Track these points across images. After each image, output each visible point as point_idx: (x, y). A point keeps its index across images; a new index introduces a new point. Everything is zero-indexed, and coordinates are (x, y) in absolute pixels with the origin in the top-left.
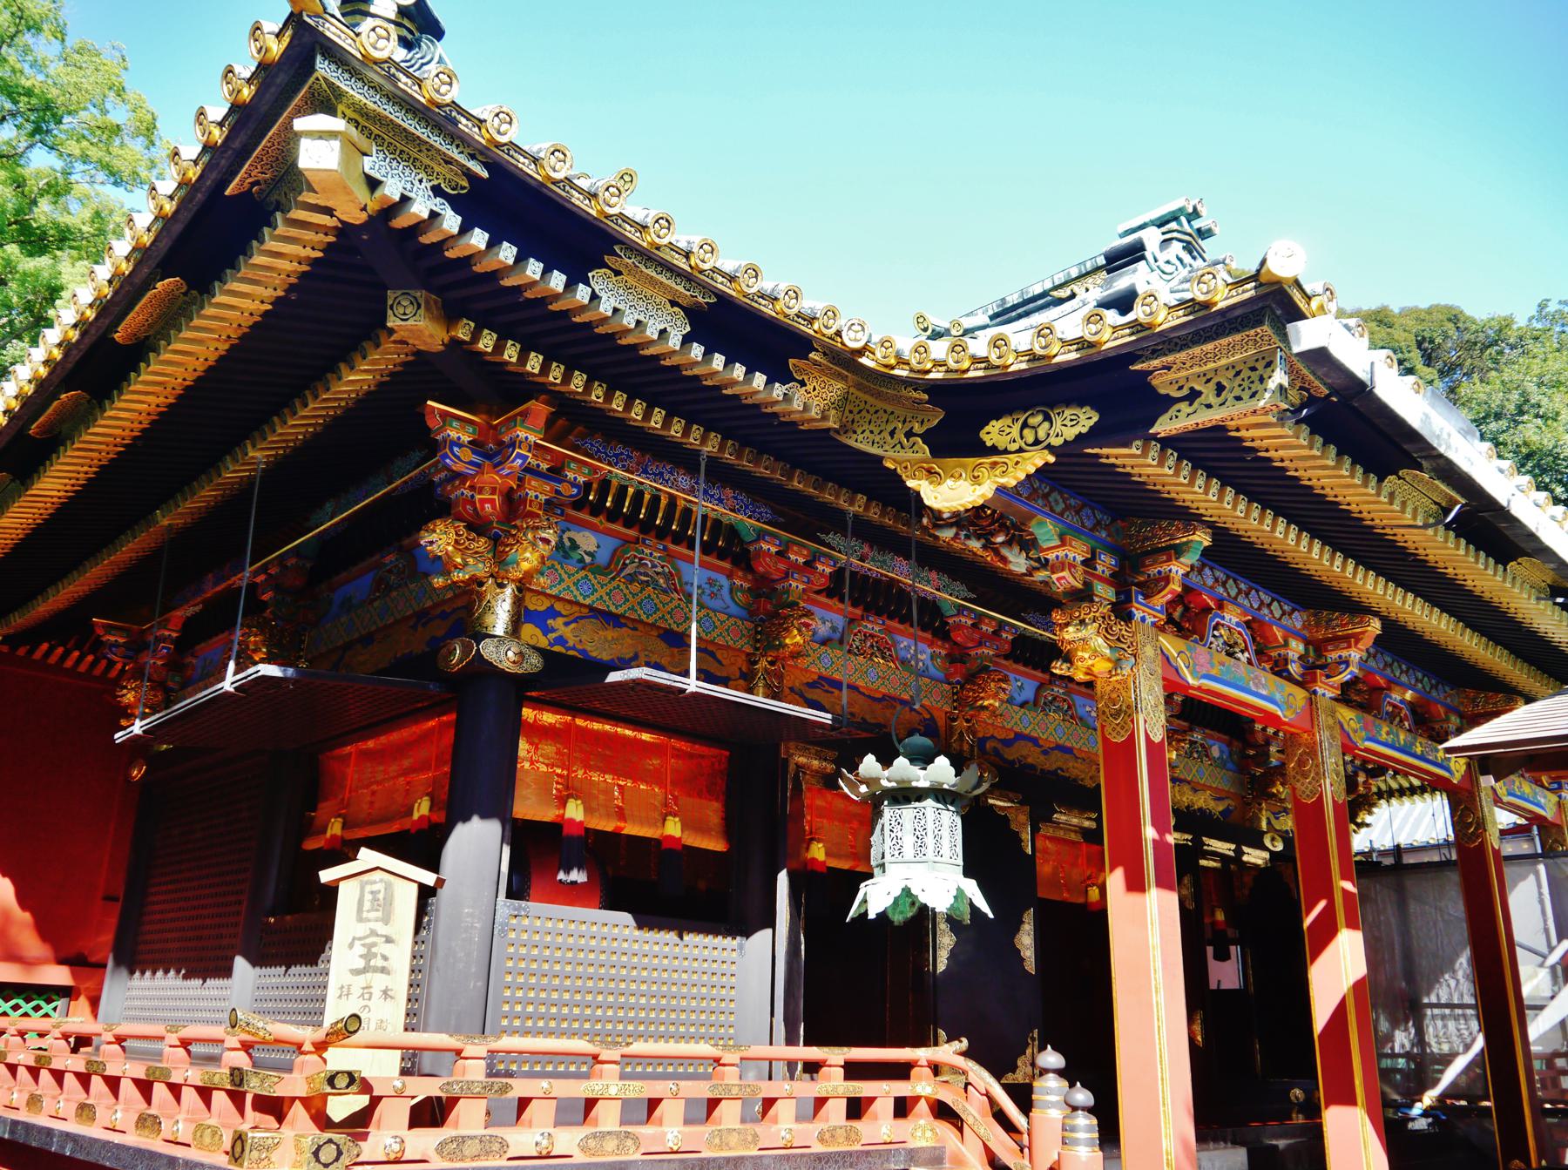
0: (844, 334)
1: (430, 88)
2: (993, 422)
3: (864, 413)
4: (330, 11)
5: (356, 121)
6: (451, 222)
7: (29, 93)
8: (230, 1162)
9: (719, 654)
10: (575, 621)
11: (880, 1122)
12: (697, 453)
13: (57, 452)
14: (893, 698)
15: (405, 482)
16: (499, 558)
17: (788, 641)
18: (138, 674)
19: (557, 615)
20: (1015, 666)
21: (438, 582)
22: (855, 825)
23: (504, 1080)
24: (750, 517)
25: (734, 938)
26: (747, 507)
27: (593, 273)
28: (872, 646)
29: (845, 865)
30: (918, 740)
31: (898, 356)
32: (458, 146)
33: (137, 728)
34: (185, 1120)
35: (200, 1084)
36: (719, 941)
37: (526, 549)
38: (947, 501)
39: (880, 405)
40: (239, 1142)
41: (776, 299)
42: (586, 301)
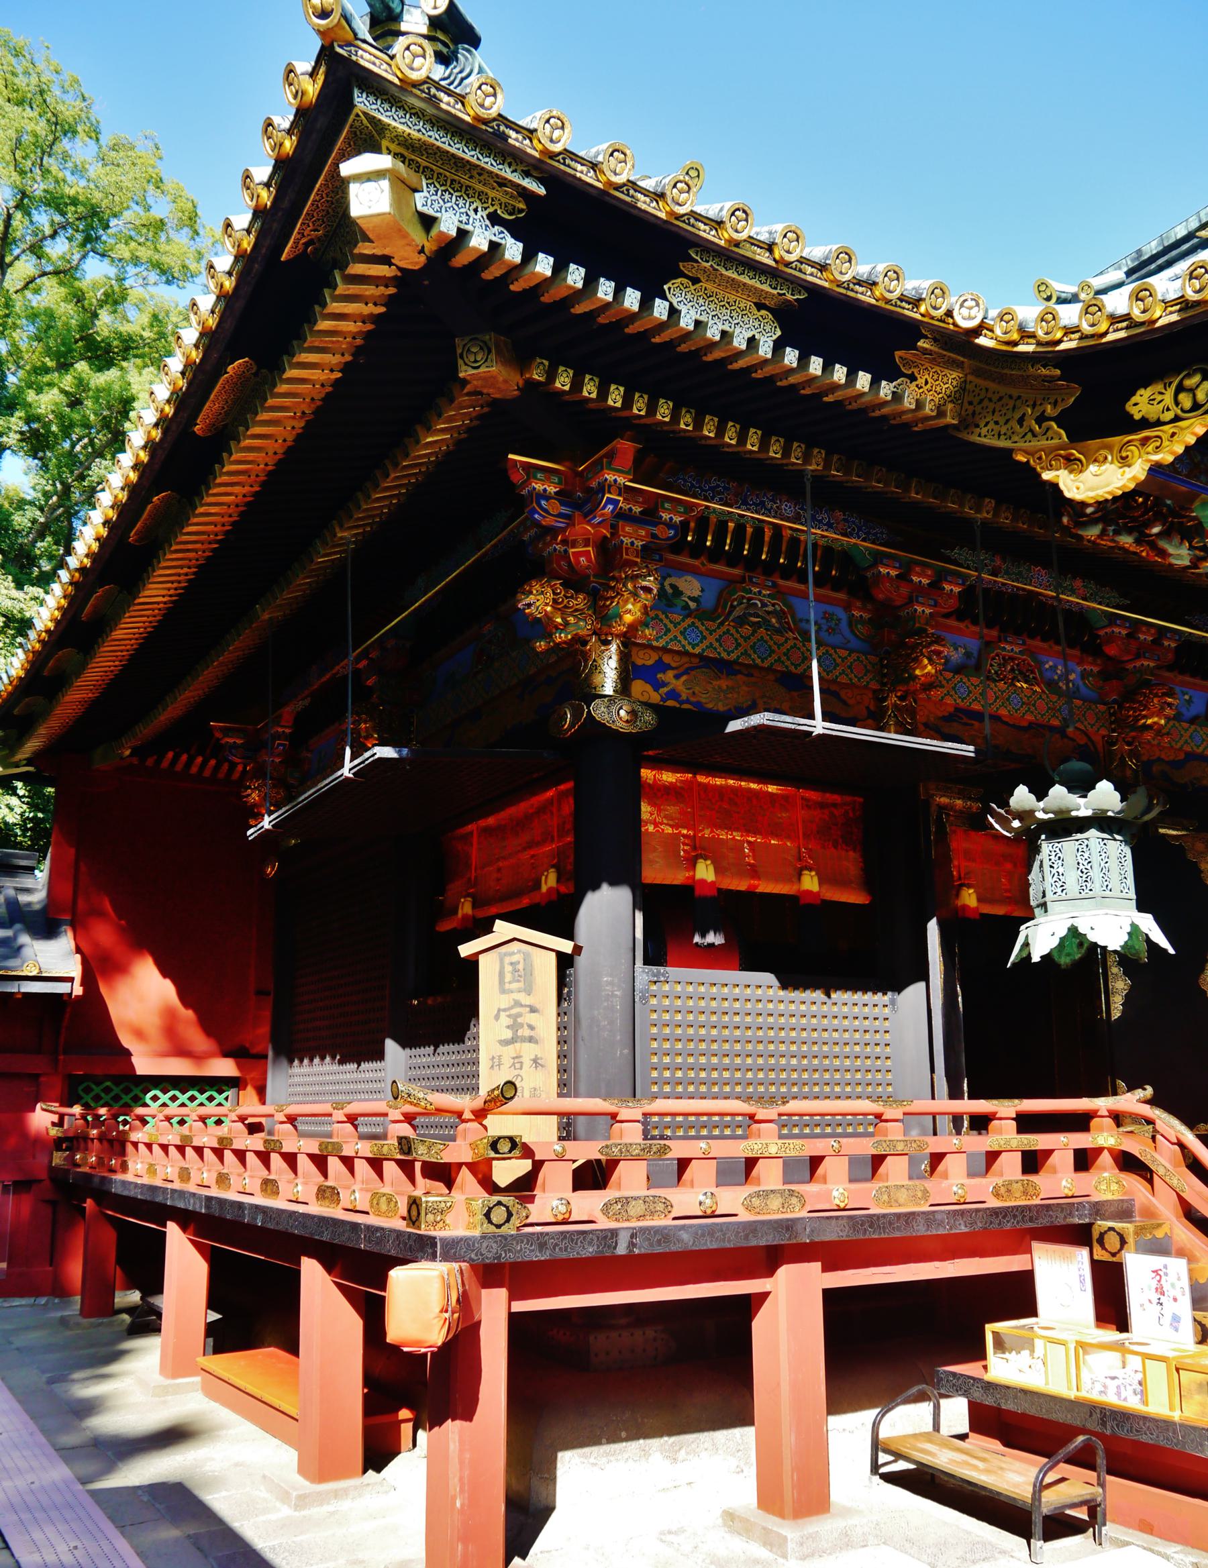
0: (955, 314)
1: (474, 104)
2: (1141, 391)
3: (986, 402)
4: (361, 36)
5: (403, 156)
6: (513, 251)
7: (74, 202)
8: (408, 1226)
9: (843, 694)
10: (685, 672)
11: (1060, 1175)
12: (800, 474)
13: (151, 564)
14: (1042, 726)
15: (495, 546)
16: (603, 617)
17: (918, 672)
18: (260, 773)
19: (666, 668)
20: (1180, 678)
21: (541, 645)
22: (1008, 866)
23: (662, 1142)
24: (864, 540)
25: (885, 994)
26: (860, 529)
27: (669, 285)
28: (1012, 670)
29: (1000, 910)
30: (1076, 765)
31: (1021, 329)
32: (510, 165)
33: (267, 823)
34: (361, 1190)
35: (371, 1155)
36: (868, 997)
37: (626, 602)
38: (1091, 489)
39: (1003, 390)
40: (414, 1207)
41: (875, 284)
42: (664, 317)
